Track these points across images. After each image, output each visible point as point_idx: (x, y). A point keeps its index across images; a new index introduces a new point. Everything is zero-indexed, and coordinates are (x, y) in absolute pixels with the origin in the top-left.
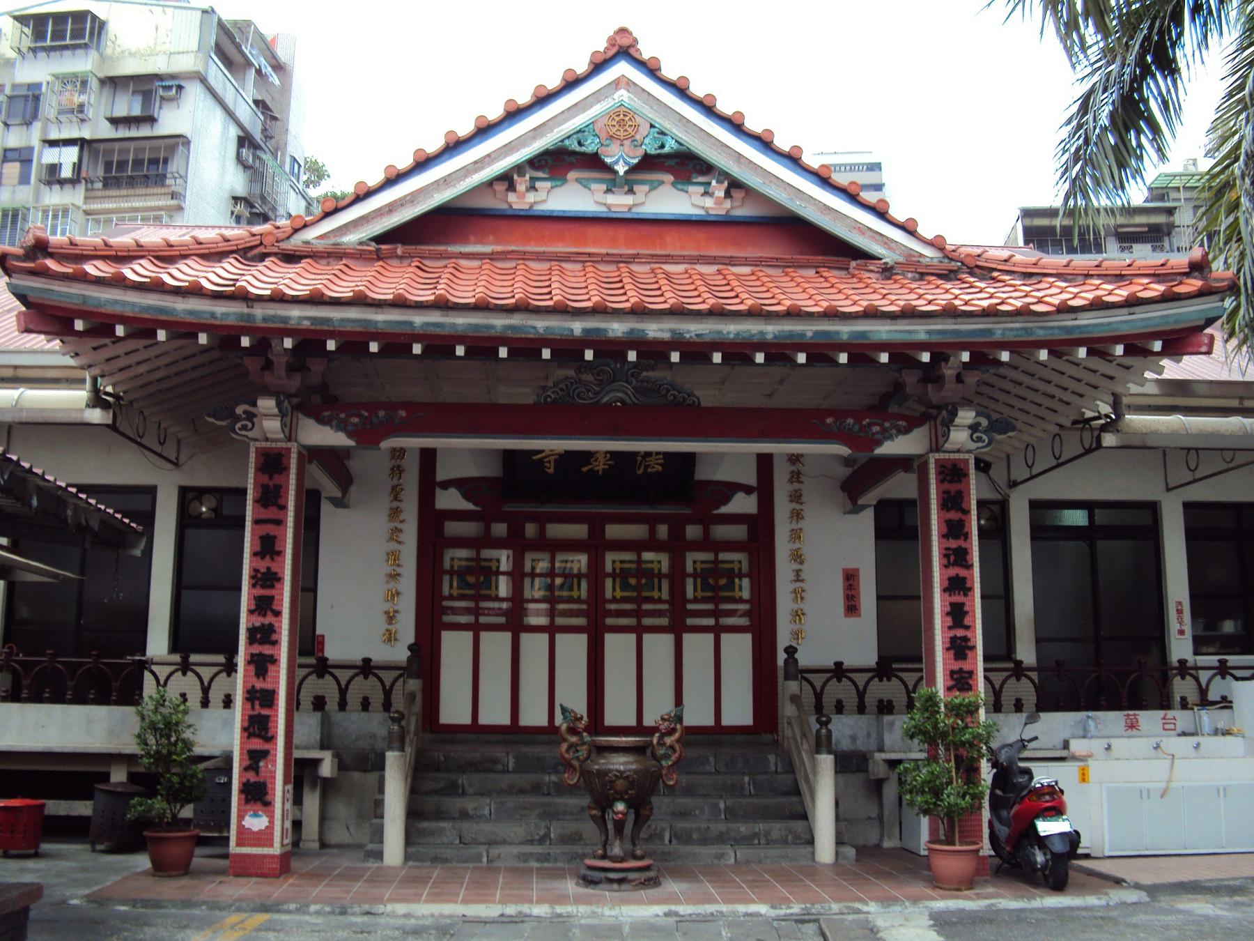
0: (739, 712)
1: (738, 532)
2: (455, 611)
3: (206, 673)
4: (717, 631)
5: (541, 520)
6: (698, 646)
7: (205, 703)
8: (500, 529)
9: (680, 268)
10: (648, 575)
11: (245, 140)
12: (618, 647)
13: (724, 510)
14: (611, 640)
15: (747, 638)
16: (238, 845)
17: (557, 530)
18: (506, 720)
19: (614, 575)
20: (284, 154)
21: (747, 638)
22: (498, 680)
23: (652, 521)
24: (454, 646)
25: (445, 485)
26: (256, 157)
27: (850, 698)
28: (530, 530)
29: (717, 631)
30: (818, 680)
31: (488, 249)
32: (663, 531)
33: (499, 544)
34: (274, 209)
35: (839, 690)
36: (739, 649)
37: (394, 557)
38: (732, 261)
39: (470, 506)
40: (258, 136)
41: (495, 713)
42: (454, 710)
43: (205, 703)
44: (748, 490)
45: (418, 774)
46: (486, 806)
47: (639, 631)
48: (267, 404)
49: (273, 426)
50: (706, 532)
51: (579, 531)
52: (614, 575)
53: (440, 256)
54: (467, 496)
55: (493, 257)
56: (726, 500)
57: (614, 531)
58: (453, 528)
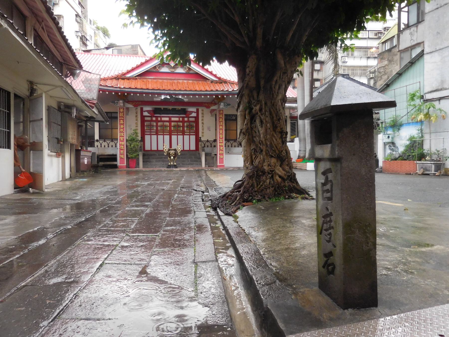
0: (193, 147)
1: (193, 119)
2: (147, 132)
3: (108, 142)
4: (190, 135)
5: (161, 117)
6: (186, 137)
7: (108, 147)
8: (154, 119)
9: (181, 81)
10: (179, 126)
11: (77, 15)
12: (174, 138)
13: (191, 116)
14: (173, 136)
15: (194, 136)
16: (124, 164)
17: (163, 119)
18: (156, 149)
19: (173, 126)
20: (87, 18)
21: (194, 136)
22: (158, 142)
23: (179, 117)
24: (147, 138)
25: (145, 111)
26: (80, 20)
27: (209, 145)
28: (159, 119)
29: (151, 135)
30: (204, 142)
31: (153, 77)
32: (181, 119)
33: (154, 121)
34: (86, 34)
35: (207, 144)
36: (193, 138)
37: (136, 123)
38: (189, 80)
39: (149, 115)
40: (80, 14)
41: (154, 148)
42: (147, 147)
43: (108, 147)
44: (195, 112)
45: (144, 155)
46: (154, 160)
47: (151, 135)
48: (121, 101)
49: (122, 104)
50: (188, 119)
51: (167, 119)
52: (173, 126)
53: (145, 79)
54: (149, 113)
55: (154, 79)
56: (191, 114)
57: (173, 119)
58: (146, 119)
